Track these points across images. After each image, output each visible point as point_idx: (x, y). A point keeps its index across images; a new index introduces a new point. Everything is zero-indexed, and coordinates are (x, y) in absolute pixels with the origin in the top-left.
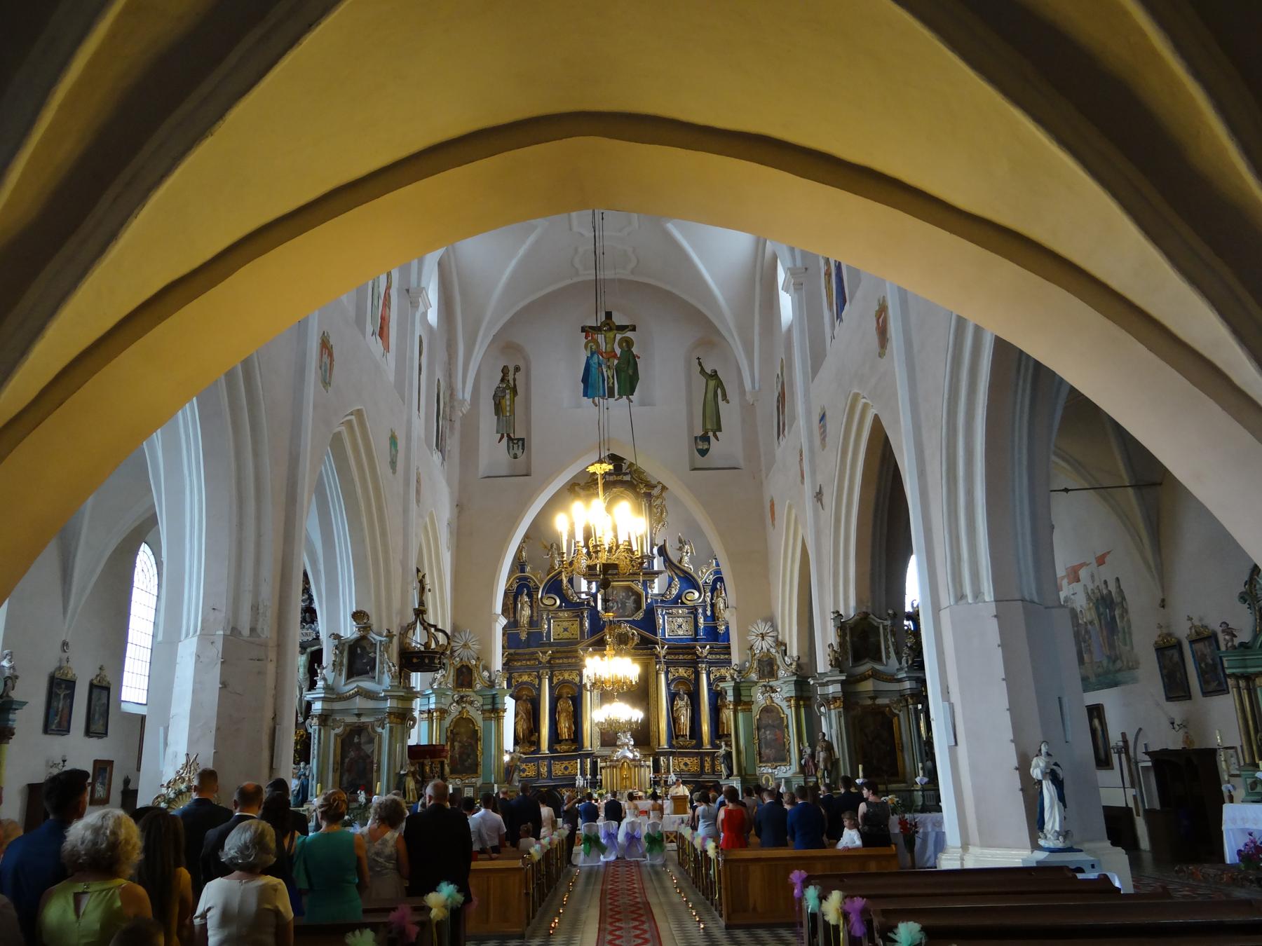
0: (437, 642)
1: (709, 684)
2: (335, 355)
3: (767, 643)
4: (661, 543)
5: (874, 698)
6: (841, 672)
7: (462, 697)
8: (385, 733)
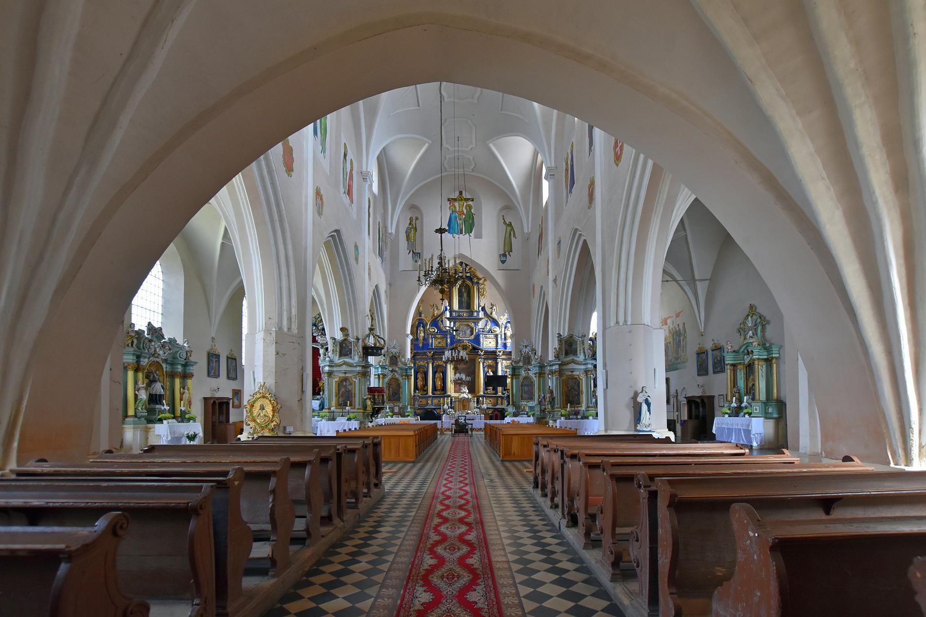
2: (324, 198)
8: (357, 381)
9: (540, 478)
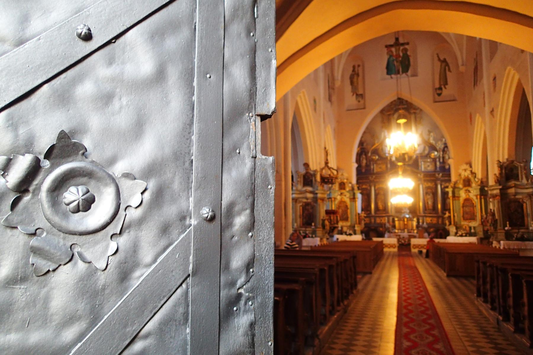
0: (333, 174)
3: (467, 174)
5: (515, 196)
9: (482, 288)
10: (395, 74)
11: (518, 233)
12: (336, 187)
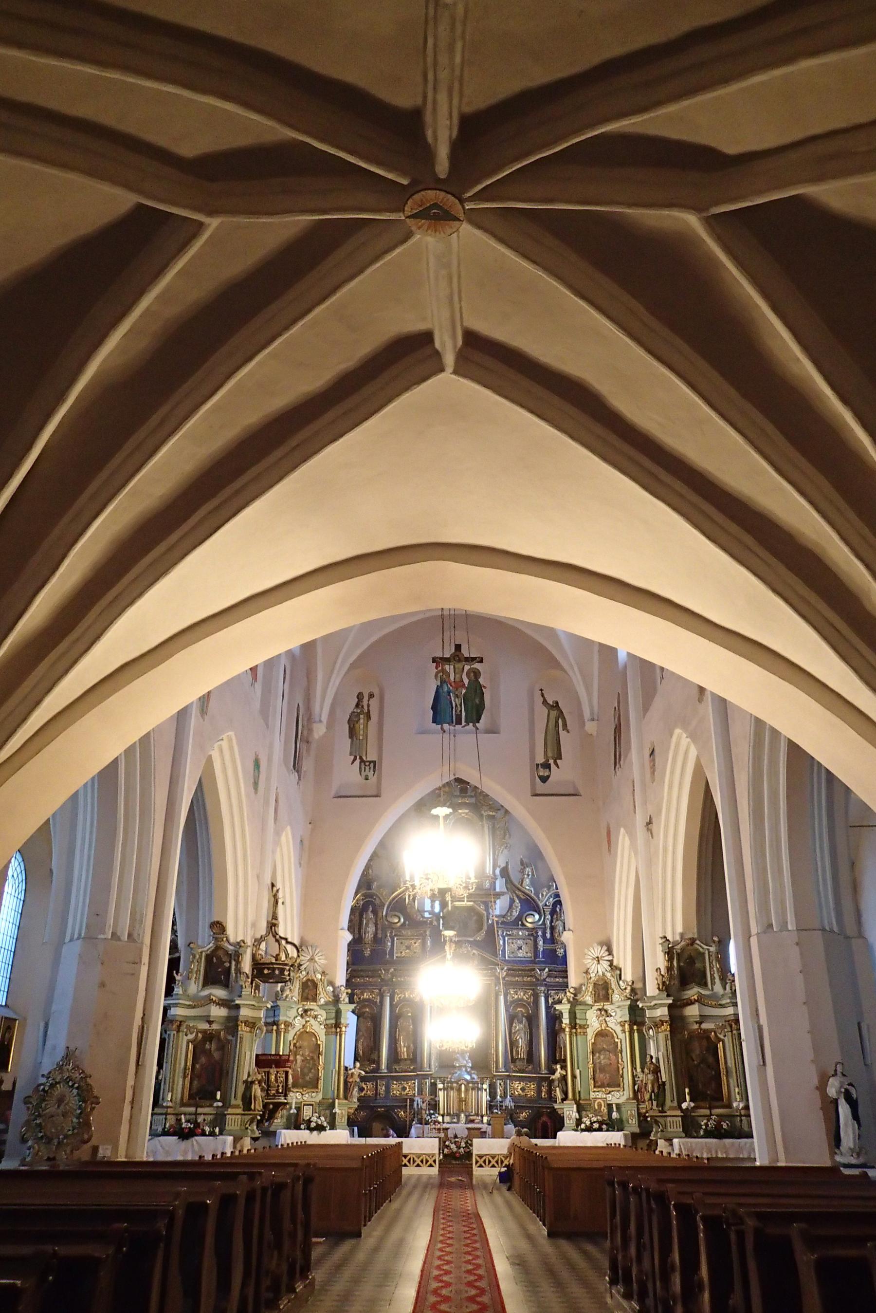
0: (287, 955)
1: (548, 1008)
4: (503, 865)
5: (700, 1023)
6: (668, 996)
7: (306, 1011)
10: (450, 723)
11: (709, 1117)
12: (293, 992)
